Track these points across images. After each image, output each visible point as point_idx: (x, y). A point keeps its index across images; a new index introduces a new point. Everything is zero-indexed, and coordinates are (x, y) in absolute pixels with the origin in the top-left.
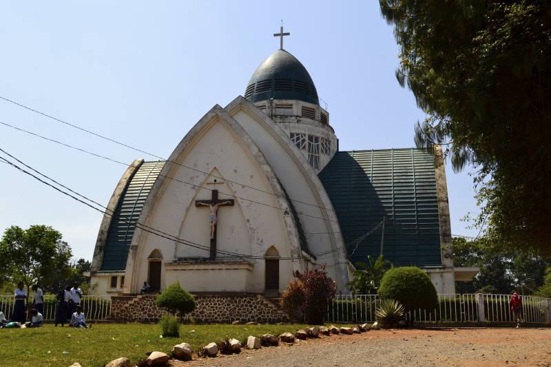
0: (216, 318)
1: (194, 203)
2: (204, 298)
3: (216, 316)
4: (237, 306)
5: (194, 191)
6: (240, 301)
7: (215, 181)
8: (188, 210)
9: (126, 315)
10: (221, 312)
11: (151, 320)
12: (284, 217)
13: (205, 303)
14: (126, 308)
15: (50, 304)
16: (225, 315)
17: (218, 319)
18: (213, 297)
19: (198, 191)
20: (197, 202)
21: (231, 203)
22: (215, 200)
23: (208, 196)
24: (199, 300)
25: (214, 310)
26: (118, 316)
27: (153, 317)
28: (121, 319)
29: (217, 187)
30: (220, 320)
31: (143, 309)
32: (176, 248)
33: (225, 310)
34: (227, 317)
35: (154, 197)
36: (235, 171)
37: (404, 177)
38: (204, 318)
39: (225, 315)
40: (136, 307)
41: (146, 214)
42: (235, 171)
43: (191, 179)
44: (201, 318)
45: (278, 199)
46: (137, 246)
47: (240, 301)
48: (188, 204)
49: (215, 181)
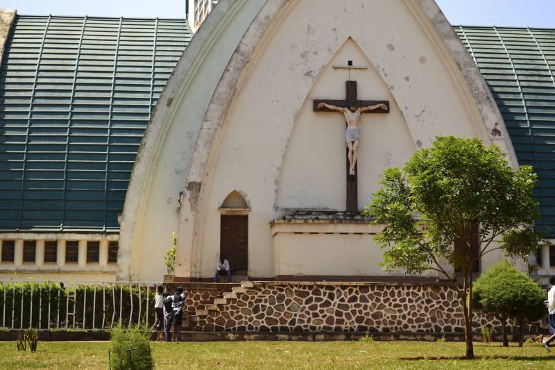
0: (406, 326)
1: (310, 105)
2: (381, 288)
3: (405, 322)
4: (446, 304)
5: (310, 79)
6: (450, 294)
7: (350, 63)
8: (297, 117)
9: (221, 321)
10: (415, 314)
11: (275, 329)
12: (491, 140)
13: (382, 298)
14: (220, 306)
15: (27, 298)
16: (423, 320)
17: (410, 329)
18: (397, 287)
19: (317, 80)
20: (316, 102)
21: (382, 108)
22: (351, 99)
23: (340, 94)
24: (370, 292)
25: (400, 311)
26: (202, 323)
27: (279, 325)
28: (209, 328)
29: (354, 76)
30: (414, 331)
31: (256, 310)
32: (276, 191)
33: (423, 311)
34: (428, 325)
35: (231, 88)
36: (391, 47)
37: (537, 78)
38: (382, 326)
39: (423, 320)
40: (240, 304)
41: (216, 121)
42: (391, 47)
43: (303, 56)
44: (375, 326)
45: (480, 106)
46: (200, 184)
47: (450, 294)
48: (298, 106)
49: (350, 63)
